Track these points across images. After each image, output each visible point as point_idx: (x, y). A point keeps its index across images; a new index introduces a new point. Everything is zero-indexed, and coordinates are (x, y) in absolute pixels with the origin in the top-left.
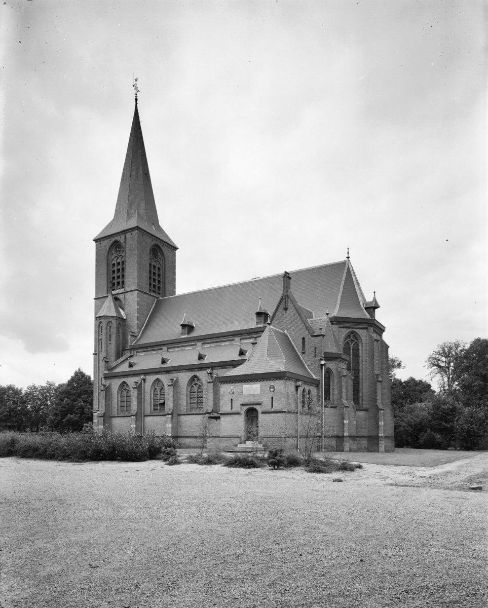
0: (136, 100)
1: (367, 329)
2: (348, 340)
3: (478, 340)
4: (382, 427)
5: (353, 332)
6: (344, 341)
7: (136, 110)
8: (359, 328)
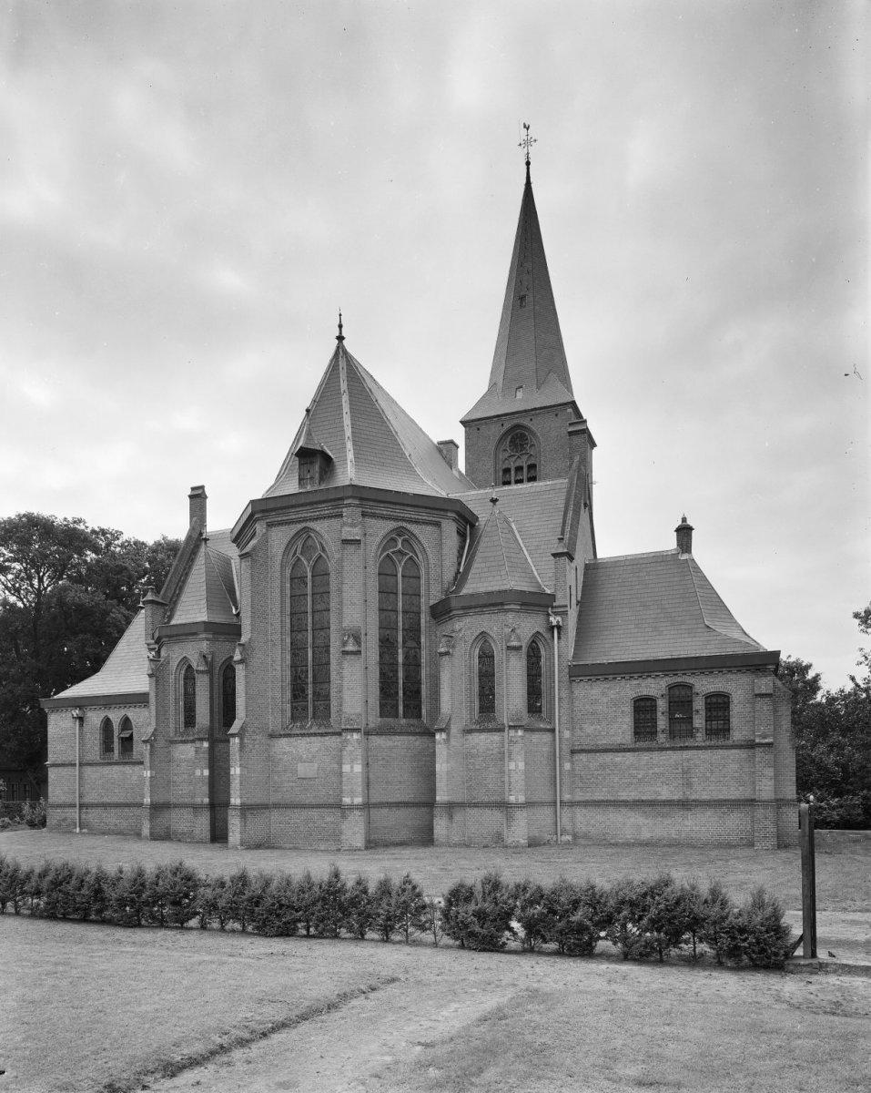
0: (528, 164)
1: (438, 524)
2: (390, 551)
3: (252, 502)
4: (237, 781)
5: (400, 531)
6: (381, 554)
7: (528, 184)
8: (417, 522)
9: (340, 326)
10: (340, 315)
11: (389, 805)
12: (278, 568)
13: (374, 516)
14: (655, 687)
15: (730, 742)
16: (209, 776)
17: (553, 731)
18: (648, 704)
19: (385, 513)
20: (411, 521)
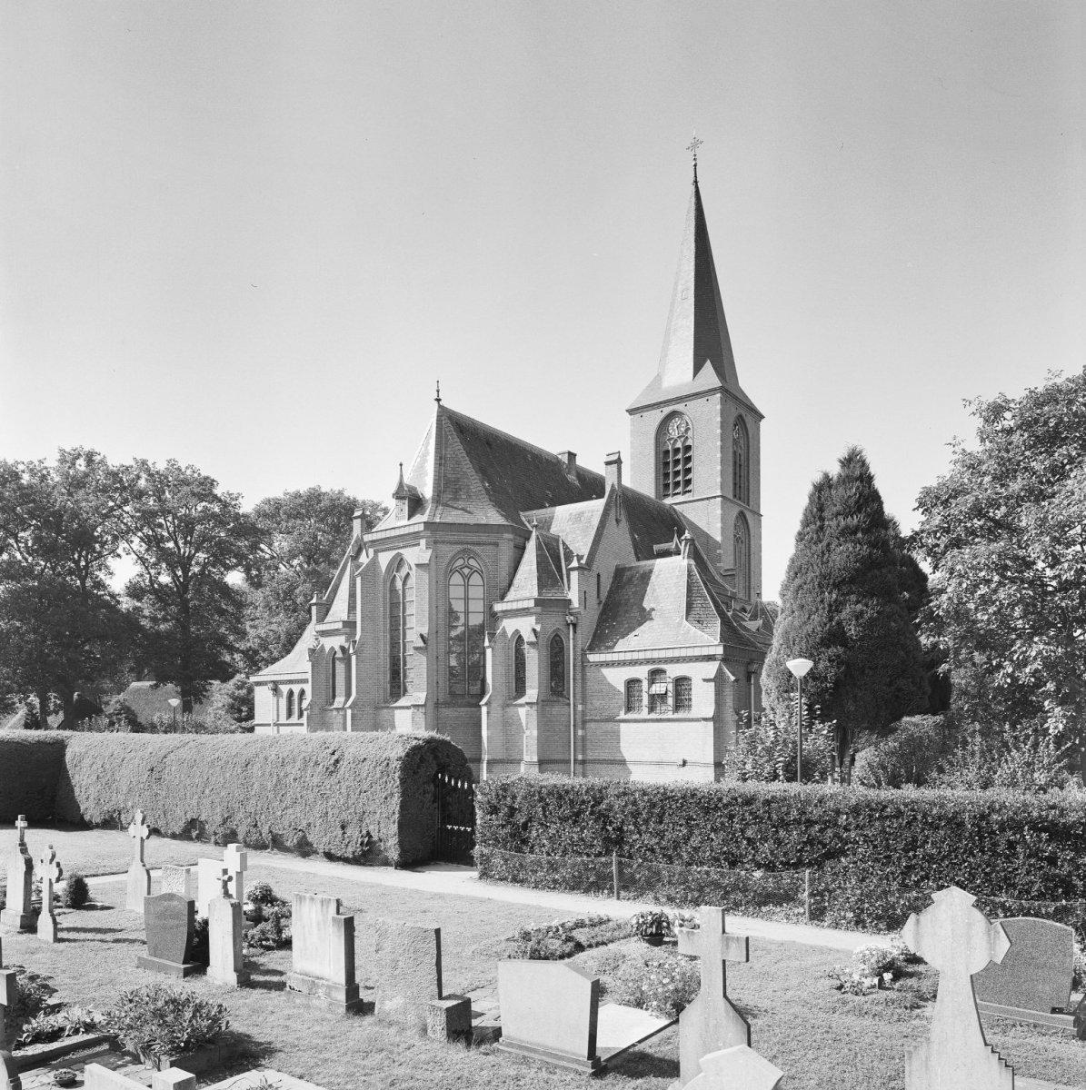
8: (478, 544)
14: (642, 672)
20: (473, 544)
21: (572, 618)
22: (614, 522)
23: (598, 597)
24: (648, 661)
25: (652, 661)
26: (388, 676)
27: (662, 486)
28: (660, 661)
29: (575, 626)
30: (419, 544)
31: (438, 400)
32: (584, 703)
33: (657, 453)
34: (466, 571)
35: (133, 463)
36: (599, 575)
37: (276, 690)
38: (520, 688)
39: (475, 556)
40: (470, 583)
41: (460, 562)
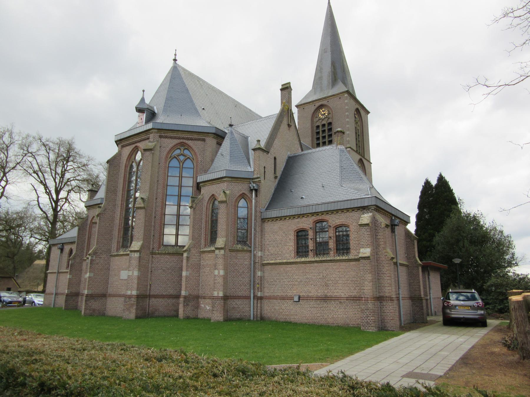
1: (204, 140)
8: (191, 139)
9: (175, 55)
10: (176, 50)
11: (163, 296)
12: (124, 166)
13: (166, 137)
14: (307, 223)
15: (351, 256)
16: (139, 278)
17: (250, 251)
18: (304, 233)
19: (172, 135)
20: (188, 139)
21: (254, 185)
22: (287, 126)
23: (275, 173)
24: (313, 214)
25: (317, 213)
26: (122, 233)
27: (315, 133)
28: (322, 213)
29: (256, 190)
30: (148, 138)
31: (175, 60)
32: (363, 376)
33: (312, 127)
34: (182, 158)
35: (36, 136)
36: (275, 158)
37: (62, 250)
38: (213, 239)
39: (188, 148)
40: (184, 166)
41: (178, 152)
